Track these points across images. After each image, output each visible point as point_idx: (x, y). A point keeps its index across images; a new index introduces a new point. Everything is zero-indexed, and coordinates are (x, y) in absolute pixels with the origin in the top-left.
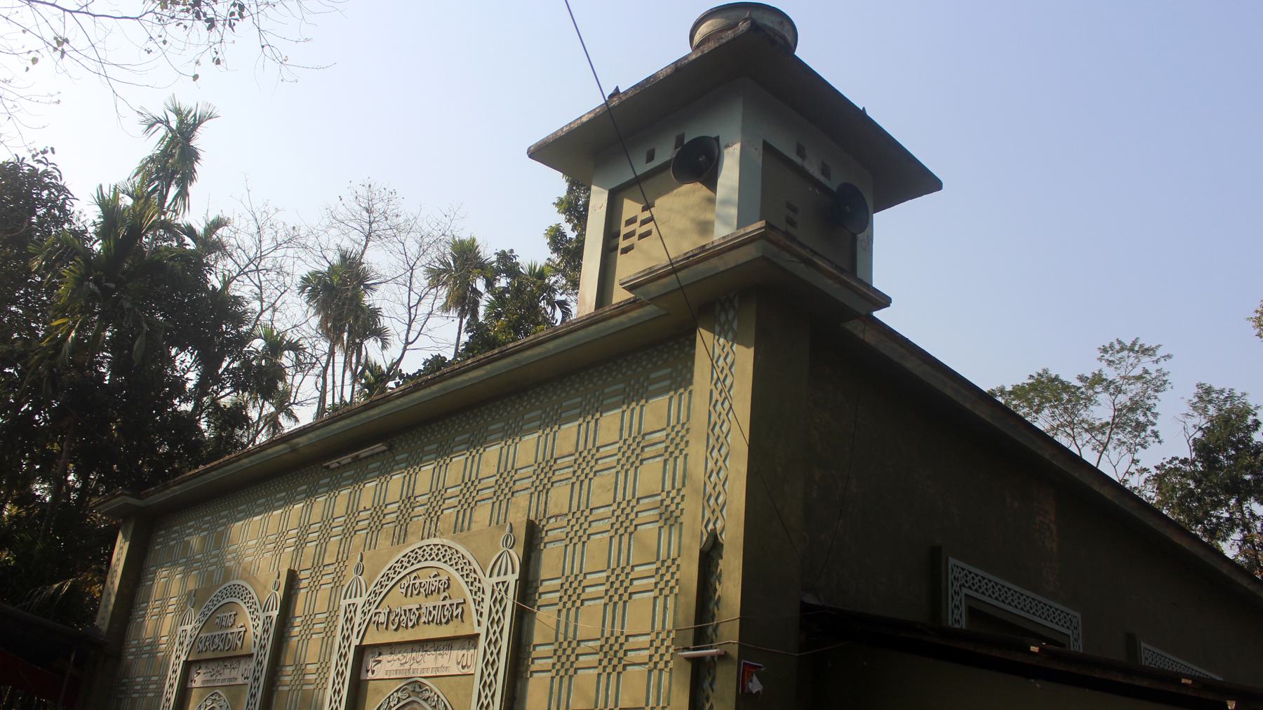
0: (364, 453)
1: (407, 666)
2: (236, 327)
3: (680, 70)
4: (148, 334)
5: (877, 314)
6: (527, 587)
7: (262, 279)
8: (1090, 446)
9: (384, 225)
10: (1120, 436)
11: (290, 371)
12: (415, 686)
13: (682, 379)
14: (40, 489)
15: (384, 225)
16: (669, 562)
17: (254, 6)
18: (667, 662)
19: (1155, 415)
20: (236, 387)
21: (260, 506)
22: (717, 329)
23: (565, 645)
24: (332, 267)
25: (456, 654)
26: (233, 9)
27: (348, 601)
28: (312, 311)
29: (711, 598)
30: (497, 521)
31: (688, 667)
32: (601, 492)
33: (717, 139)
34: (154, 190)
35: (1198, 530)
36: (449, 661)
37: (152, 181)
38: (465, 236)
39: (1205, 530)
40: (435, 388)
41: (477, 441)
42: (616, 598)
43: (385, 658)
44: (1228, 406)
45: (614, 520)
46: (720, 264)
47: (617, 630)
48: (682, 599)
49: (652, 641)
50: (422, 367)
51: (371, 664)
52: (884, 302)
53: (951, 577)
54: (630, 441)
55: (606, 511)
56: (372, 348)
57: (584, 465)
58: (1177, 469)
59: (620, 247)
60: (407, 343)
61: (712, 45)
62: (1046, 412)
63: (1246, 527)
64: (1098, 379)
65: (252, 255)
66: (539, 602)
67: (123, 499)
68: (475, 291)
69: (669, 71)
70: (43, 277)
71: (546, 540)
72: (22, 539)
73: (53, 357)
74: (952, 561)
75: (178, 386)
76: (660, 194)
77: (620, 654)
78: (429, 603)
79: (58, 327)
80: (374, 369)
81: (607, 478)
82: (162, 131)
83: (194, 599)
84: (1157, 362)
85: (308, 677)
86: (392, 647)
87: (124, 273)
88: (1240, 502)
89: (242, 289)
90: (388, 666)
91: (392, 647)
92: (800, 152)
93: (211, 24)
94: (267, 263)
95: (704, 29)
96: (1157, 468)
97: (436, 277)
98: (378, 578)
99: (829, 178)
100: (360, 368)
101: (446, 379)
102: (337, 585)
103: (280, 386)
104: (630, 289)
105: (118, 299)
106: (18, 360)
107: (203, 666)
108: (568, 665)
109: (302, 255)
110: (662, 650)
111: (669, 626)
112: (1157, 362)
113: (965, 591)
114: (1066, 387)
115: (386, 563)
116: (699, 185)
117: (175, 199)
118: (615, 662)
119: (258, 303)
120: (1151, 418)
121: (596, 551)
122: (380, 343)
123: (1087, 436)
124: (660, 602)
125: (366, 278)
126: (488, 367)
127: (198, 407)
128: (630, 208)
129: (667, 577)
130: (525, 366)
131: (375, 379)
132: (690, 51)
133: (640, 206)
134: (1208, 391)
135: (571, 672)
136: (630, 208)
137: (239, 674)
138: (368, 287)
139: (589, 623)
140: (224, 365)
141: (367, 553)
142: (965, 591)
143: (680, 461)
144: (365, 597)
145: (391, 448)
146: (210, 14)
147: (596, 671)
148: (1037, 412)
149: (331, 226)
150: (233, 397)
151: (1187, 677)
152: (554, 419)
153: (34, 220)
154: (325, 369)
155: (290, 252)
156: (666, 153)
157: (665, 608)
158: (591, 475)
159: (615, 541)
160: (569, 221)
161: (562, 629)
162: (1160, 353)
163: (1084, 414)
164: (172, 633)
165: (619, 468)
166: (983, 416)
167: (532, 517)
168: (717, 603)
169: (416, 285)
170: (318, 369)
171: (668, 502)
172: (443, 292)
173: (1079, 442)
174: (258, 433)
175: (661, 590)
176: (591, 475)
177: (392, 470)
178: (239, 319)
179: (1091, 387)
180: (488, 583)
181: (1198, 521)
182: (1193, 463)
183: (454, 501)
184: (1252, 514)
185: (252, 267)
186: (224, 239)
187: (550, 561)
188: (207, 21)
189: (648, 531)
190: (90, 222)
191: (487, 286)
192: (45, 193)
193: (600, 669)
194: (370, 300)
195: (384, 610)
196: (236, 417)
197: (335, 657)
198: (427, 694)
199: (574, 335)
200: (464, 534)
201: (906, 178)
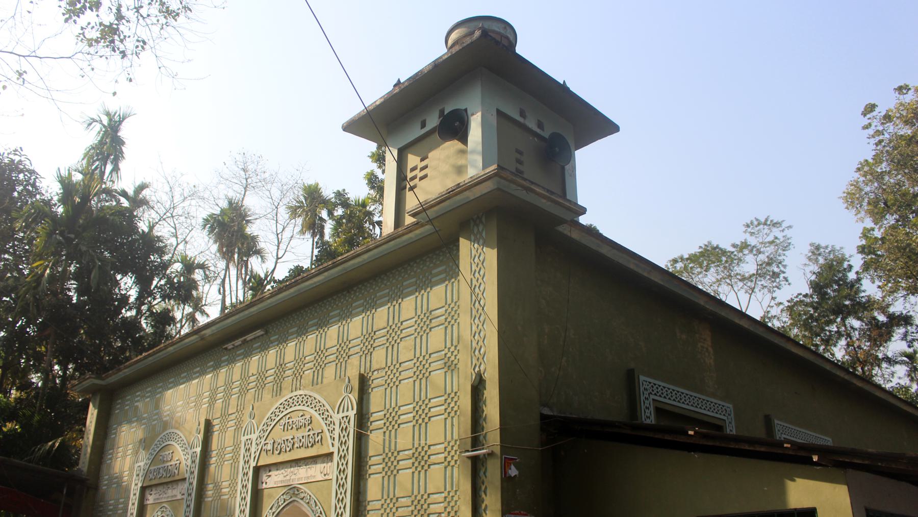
0: (249, 337)
1: (288, 478)
2: (161, 257)
3: (437, 66)
4: (100, 267)
6: (362, 418)
8: (743, 291)
9: (255, 179)
10: (763, 282)
11: (200, 283)
12: (293, 490)
13: (452, 272)
14: (35, 378)
15: (255, 179)
16: (453, 395)
17: (151, 41)
18: (456, 461)
19: (785, 266)
20: (164, 298)
21: (183, 378)
22: (473, 238)
23: (390, 455)
24: (223, 211)
25: (319, 467)
26: (137, 44)
27: (246, 437)
28: (211, 241)
29: (481, 416)
30: (340, 377)
31: (469, 462)
32: (405, 351)
33: (466, 110)
34: (96, 168)
35: (817, 341)
36: (315, 472)
37: (94, 161)
38: (311, 182)
39: (822, 340)
40: (292, 290)
41: (323, 323)
42: (420, 421)
43: (273, 473)
44: (832, 256)
45: (415, 369)
46: (471, 195)
47: (423, 442)
48: (462, 419)
49: (445, 448)
50: (287, 275)
51: (264, 478)
52: (583, 211)
53: (642, 389)
54: (422, 316)
55: (411, 364)
57: (393, 334)
58: (801, 301)
59: (408, 186)
60: (278, 258)
61: (457, 48)
62: (712, 270)
64: (744, 246)
65: (168, 207)
66: (371, 428)
67: (91, 380)
68: (321, 219)
69: (431, 67)
70: (25, 233)
71: (373, 386)
72: (24, 414)
73: (35, 288)
75: (124, 299)
76: (431, 150)
78: (299, 434)
79: (37, 267)
80: (254, 276)
81: (409, 341)
82: (97, 127)
83: (145, 443)
84: (783, 231)
85: (224, 490)
87: (79, 227)
88: (843, 320)
89: (163, 231)
92: (522, 114)
93: (124, 54)
94: (178, 211)
95: (454, 36)
96: (788, 301)
97: (294, 212)
99: (543, 130)
100: (248, 277)
101: (299, 284)
102: (238, 427)
103: (194, 293)
104: (414, 215)
105: (77, 244)
106: (12, 291)
107: (154, 489)
108: (392, 468)
109: (201, 204)
110: (453, 453)
111: (456, 437)
112: (783, 231)
113: (652, 397)
114: (724, 252)
116: (456, 142)
117: (111, 173)
119: (174, 239)
120: (782, 269)
122: (260, 259)
123: (740, 284)
124: (449, 421)
125: (246, 215)
126: (326, 274)
127: (139, 312)
128: (413, 160)
129: (452, 404)
130: (358, 271)
131: (256, 284)
132: (446, 51)
133: (419, 159)
134: (818, 248)
135: (395, 472)
137: (177, 492)
138: (248, 221)
139: (404, 439)
140: (155, 283)
143: (455, 327)
144: (257, 434)
145: (267, 332)
146: (122, 48)
149: (219, 183)
150: (163, 304)
153: (16, 194)
154: (224, 281)
155: (193, 202)
156: (433, 121)
157: (452, 425)
158: (398, 341)
162: (784, 225)
163: (737, 269)
164: (131, 469)
165: (416, 334)
166: (656, 280)
167: (362, 372)
168: (485, 419)
169: (280, 218)
170: (219, 281)
171: (449, 355)
172: (299, 221)
173: (736, 289)
174: (182, 327)
176: (398, 341)
177: (269, 347)
178: (161, 251)
179: (741, 251)
180: (336, 418)
181: (817, 335)
182: (811, 296)
183: (311, 365)
184: (852, 328)
186: (148, 197)
188: (121, 52)
189: (438, 376)
190: (54, 193)
191: (328, 216)
192: (21, 176)
194: (250, 230)
196: (164, 319)
197: (240, 475)
198: (302, 495)
199: (380, 249)
201: (596, 126)
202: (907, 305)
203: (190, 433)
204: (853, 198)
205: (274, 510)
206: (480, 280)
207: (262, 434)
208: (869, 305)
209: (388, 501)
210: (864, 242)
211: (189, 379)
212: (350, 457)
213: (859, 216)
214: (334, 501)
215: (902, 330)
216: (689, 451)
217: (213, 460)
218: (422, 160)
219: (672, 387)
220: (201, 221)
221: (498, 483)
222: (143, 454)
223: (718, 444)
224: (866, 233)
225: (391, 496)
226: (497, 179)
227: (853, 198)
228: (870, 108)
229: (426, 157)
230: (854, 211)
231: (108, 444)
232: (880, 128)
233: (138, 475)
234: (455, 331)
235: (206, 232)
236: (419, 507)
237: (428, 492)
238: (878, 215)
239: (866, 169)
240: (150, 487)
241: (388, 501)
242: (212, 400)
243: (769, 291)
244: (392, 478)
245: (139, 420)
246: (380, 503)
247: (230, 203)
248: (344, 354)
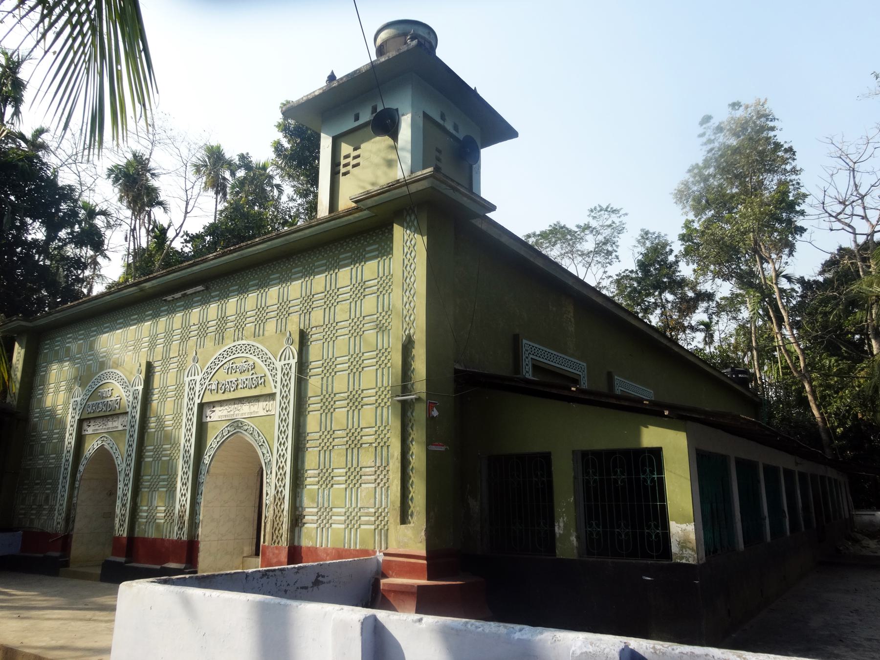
0: (189, 291)
1: (232, 413)
5: (490, 215)
6: (303, 366)
7: (80, 169)
10: (598, 259)
12: (236, 424)
13: (385, 250)
19: (617, 246)
21: (120, 323)
22: (405, 225)
23: (327, 396)
25: (262, 404)
27: (190, 378)
29: (409, 369)
31: (399, 406)
32: (341, 312)
33: (397, 110)
36: (258, 408)
40: (235, 254)
42: (355, 370)
43: (217, 409)
44: (657, 241)
50: (202, 230)
51: (208, 413)
52: (492, 208)
58: (628, 276)
60: (186, 213)
61: (392, 54)
62: (558, 246)
63: (663, 307)
64: (587, 227)
66: (310, 374)
68: (224, 179)
74: (524, 341)
76: (363, 141)
78: (243, 377)
86: (221, 403)
88: (660, 294)
90: (220, 414)
91: (221, 403)
92: (443, 117)
95: (383, 35)
100: (151, 227)
102: (181, 369)
104: (356, 202)
108: (329, 407)
111: (385, 384)
113: (531, 356)
114: (570, 232)
115: (213, 356)
116: (387, 137)
118: (356, 403)
121: (342, 345)
123: (580, 259)
124: (379, 372)
126: (269, 243)
128: (346, 149)
134: (647, 233)
135: (332, 410)
136: (346, 149)
139: (340, 384)
141: (199, 351)
142: (531, 356)
144: (201, 375)
145: (207, 288)
147: (346, 409)
148: (553, 246)
151: (647, 400)
152: (310, 272)
156: (366, 116)
159: (352, 339)
160: (285, 137)
161: (325, 388)
162: (621, 212)
163: (578, 246)
164: (66, 404)
167: (302, 327)
168: (413, 372)
175: (380, 365)
177: (210, 301)
179: (583, 231)
180: (279, 365)
181: (638, 304)
184: (666, 300)
185: (70, 161)
187: (315, 351)
189: (370, 335)
193: (348, 408)
194: (154, 183)
197: (185, 411)
198: (246, 428)
199: (322, 226)
200: (261, 337)
201: (498, 130)
202: (714, 286)
203: (131, 373)
204: (682, 195)
206: (411, 261)
207: (206, 376)
208: (683, 283)
210: (684, 231)
211: (126, 325)
212: (292, 397)
213: (684, 210)
214: (276, 433)
215: (705, 304)
216: (569, 402)
217: (155, 397)
218: (355, 149)
220: (106, 171)
222: (77, 389)
223: (592, 398)
224: (687, 225)
225: (329, 429)
226: (431, 179)
227: (682, 195)
229: (359, 148)
230: (680, 206)
234: (390, 297)
235: (110, 181)
236: (353, 438)
237: (361, 426)
238: (699, 211)
241: (326, 433)
242: (152, 346)
243: (603, 266)
244: (329, 415)
245: (72, 359)
246: (319, 434)
247: (135, 155)
248: (284, 310)
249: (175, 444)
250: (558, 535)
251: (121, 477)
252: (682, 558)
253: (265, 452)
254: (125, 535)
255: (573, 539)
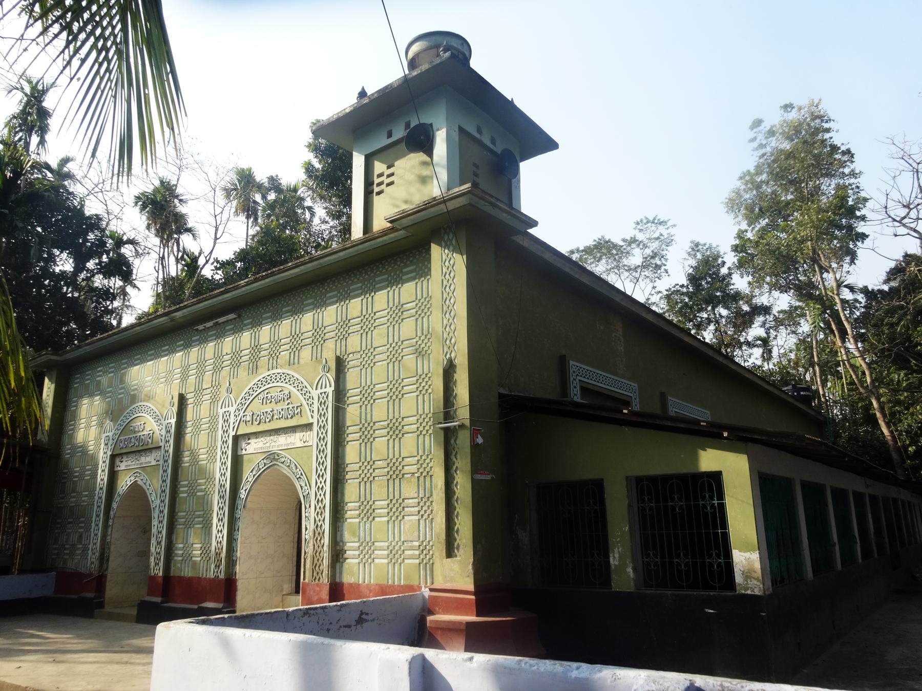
0: (221, 320)
1: (268, 445)
6: (340, 394)
10: (646, 273)
12: (272, 457)
13: (423, 270)
19: (666, 260)
21: (151, 355)
22: (443, 244)
23: (366, 425)
29: (451, 395)
32: (379, 337)
33: (431, 125)
34: (20, 139)
35: (690, 325)
36: (295, 439)
38: (245, 166)
39: (695, 325)
40: (267, 280)
41: (297, 311)
43: (252, 441)
44: (708, 253)
47: (397, 415)
50: (233, 257)
51: (244, 445)
52: (534, 223)
54: (394, 308)
56: (186, 240)
58: (678, 291)
60: (216, 239)
62: (604, 261)
64: (633, 241)
66: (348, 402)
68: (255, 202)
77: (400, 428)
78: (279, 407)
86: (256, 435)
87: (12, 202)
88: (713, 309)
90: (256, 446)
91: (256, 435)
92: (479, 131)
95: (415, 48)
97: (228, 193)
98: (243, 395)
100: (180, 254)
102: (214, 400)
104: (391, 222)
110: (424, 424)
111: (427, 411)
113: (579, 378)
114: (615, 246)
116: (421, 153)
121: (380, 372)
123: (627, 274)
124: (420, 398)
126: (302, 267)
128: (379, 167)
133: (385, 166)
134: (697, 245)
135: (371, 440)
136: (379, 167)
139: (380, 412)
141: (232, 381)
142: (579, 378)
144: (235, 407)
145: (239, 316)
147: (386, 438)
148: (598, 261)
152: (346, 296)
156: (399, 133)
157: (424, 401)
161: (363, 417)
162: (669, 224)
163: (625, 261)
167: (338, 354)
179: (629, 245)
180: (315, 393)
181: (690, 321)
184: (720, 314)
185: (96, 190)
187: (352, 378)
189: (409, 360)
193: (389, 437)
194: (182, 209)
195: (248, 413)
197: (219, 443)
198: (283, 460)
199: (356, 248)
201: (541, 143)
202: (771, 299)
203: (163, 406)
204: (733, 204)
205: (254, 473)
206: (450, 281)
208: (737, 296)
209: (366, 464)
210: (737, 242)
211: (157, 356)
212: (329, 427)
213: (737, 220)
214: (314, 464)
215: (761, 319)
216: (621, 425)
217: (189, 430)
218: (389, 167)
219: (600, 372)
221: (467, 449)
222: (108, 423)
224: (740, 235)
225: (368, 459)
227: (733, 204)
228: (758, 123)
231: (69, 415)
232: (764, 142)
233: (106, 444)
234: (427, 322)
235: (138, 209)
236: (394, 468)
237: (402, 456)
238: (752, 220)
239: (747, 178)
240: (121, 455)
241: (366, 464)
242: (184, 377)
244: (368, 445)
245: (103, 393)
246: (358, 465)
247: (162, 182)
249: (210, 478)
250: (613, 567)
251: (155, 514)
252: (747, 589)
253: (303, 485)
254: (161, 574)
255: (630, 570)
